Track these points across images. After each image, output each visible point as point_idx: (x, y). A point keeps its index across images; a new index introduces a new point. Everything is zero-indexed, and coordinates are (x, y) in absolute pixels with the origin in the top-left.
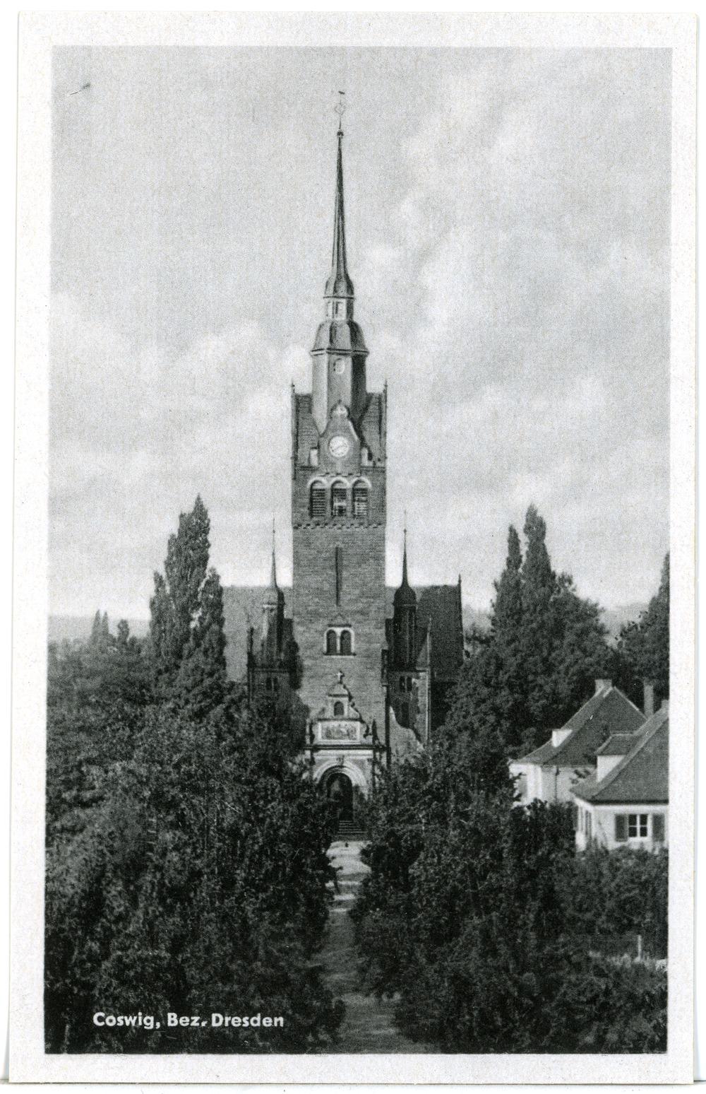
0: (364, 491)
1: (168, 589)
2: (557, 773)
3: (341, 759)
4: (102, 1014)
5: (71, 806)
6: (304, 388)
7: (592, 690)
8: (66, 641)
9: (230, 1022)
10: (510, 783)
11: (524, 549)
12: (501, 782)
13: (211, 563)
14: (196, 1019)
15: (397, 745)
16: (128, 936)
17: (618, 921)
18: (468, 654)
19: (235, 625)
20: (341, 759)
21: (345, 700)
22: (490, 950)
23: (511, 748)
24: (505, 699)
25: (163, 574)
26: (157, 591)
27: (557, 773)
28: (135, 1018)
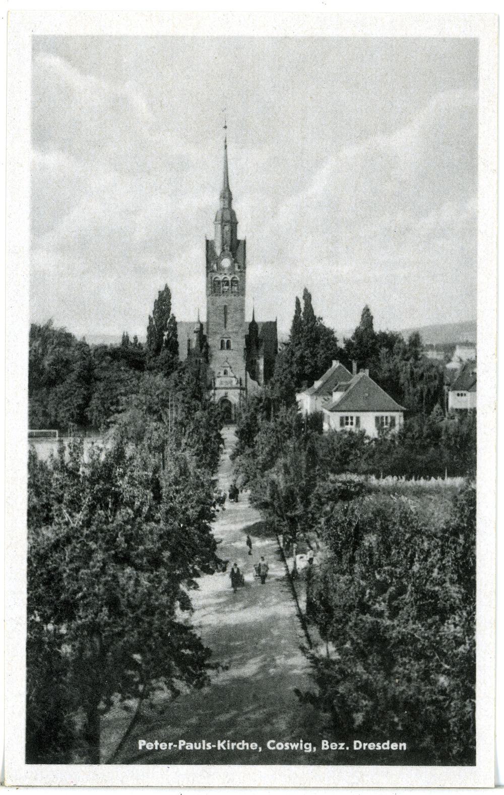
0: (237, 282)
1: (154, 323)
2: (316, 399)
3: (226, 394)
4: (273, 741)
5: (114, 413)
6: (211, 237)
7: (331, 365)
8: (111, 345)
9: (367, 747)
10: (296, 404)
11: (302, 306)
12: (291, 401)
13: (172, 312)
14: (342, 744)
15: (249, 387)
16: (134, 466)
17: (340, 461)
18: (280, 350)
19: (182, 339)
20: (226, 394)
21: (228, 369)
22: (287, 472)
23: (297, 389)
24: (295, 369)
25: (152, 316)
26: (150, 323)
27: (316, 399)
28: (298, 744)
